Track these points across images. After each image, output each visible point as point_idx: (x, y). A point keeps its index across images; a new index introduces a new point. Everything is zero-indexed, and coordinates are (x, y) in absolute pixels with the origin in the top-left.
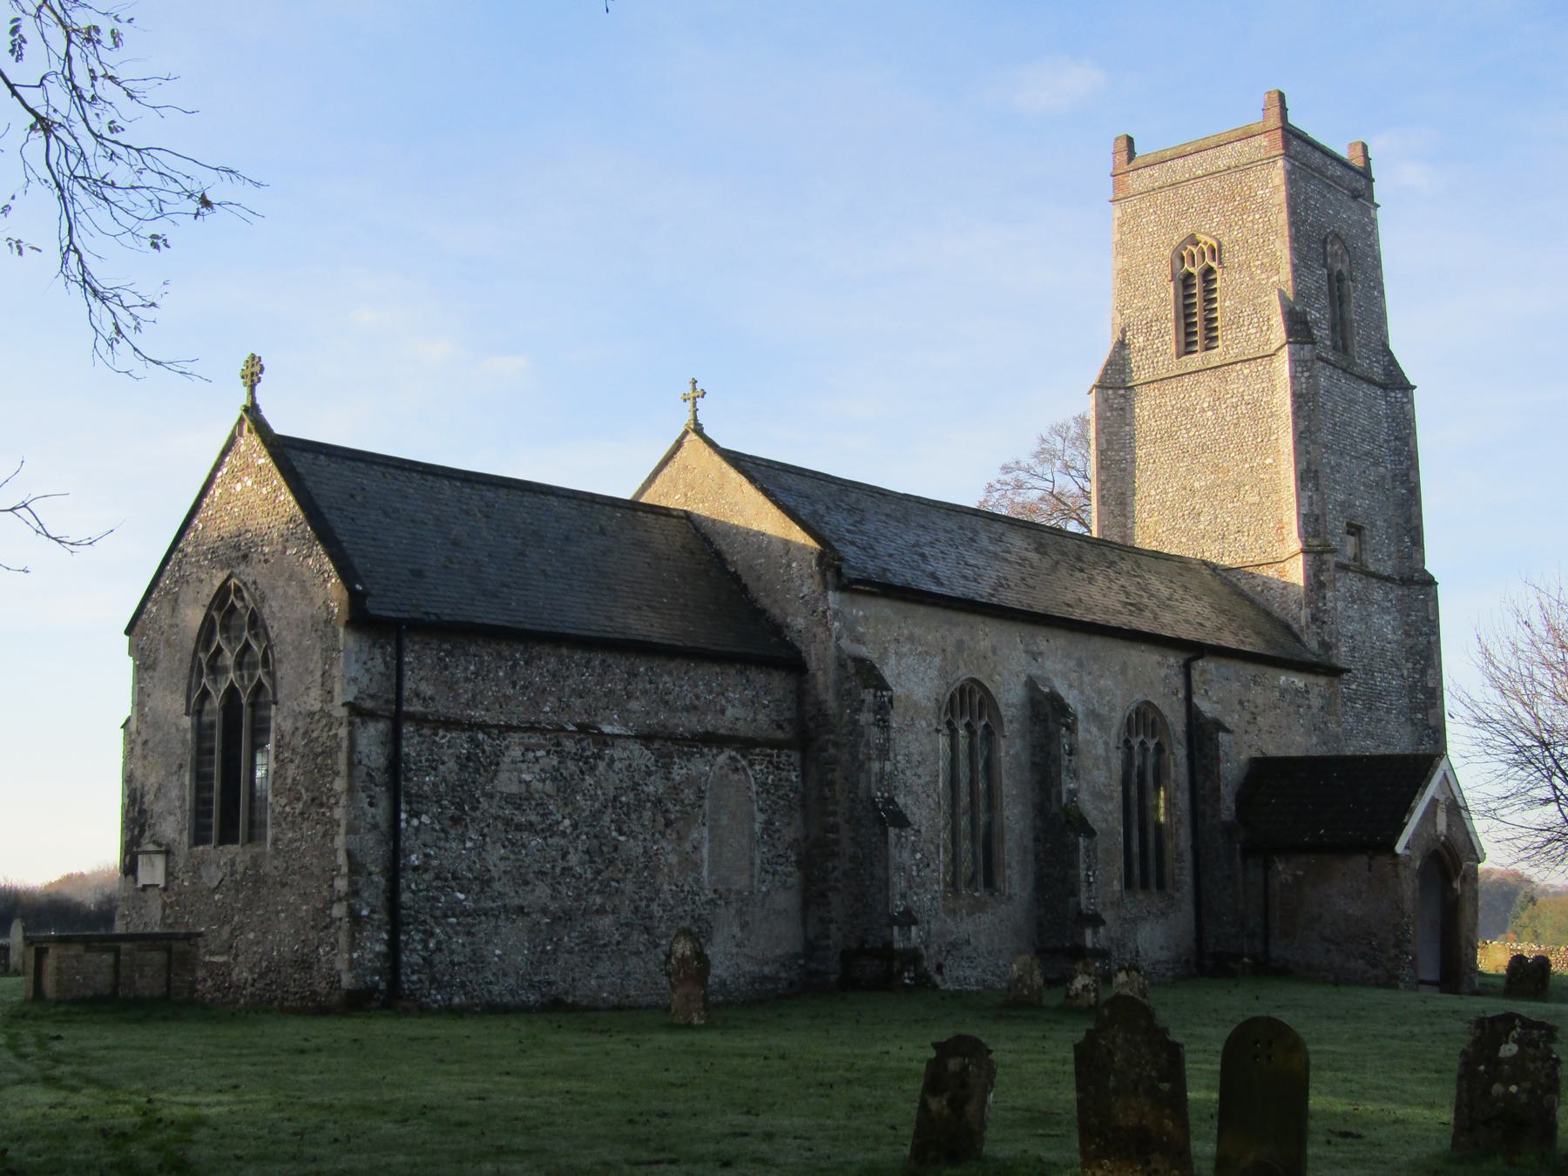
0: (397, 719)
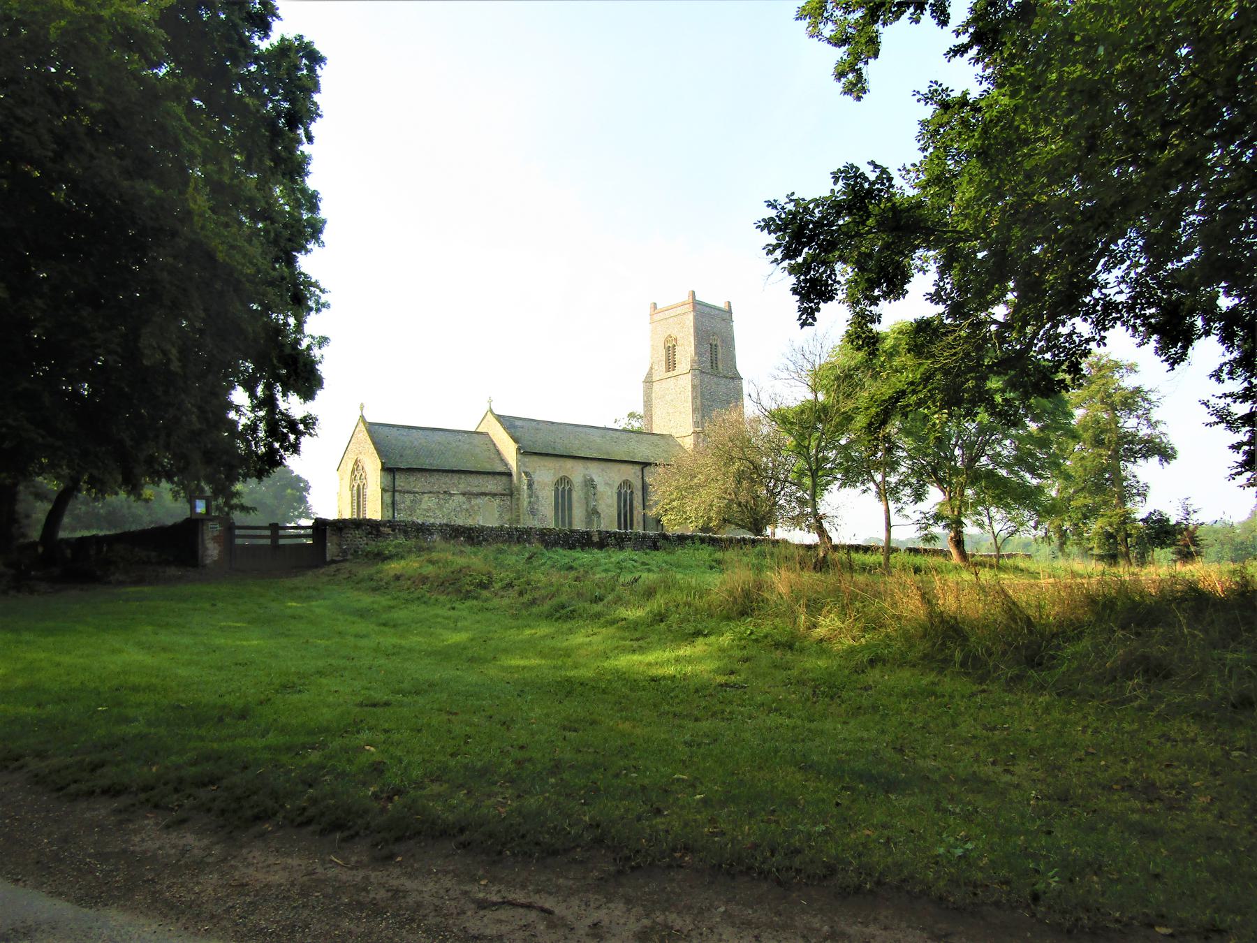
0: (394, 491)
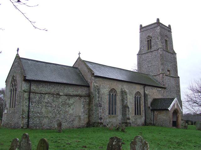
0: (30, 92)
